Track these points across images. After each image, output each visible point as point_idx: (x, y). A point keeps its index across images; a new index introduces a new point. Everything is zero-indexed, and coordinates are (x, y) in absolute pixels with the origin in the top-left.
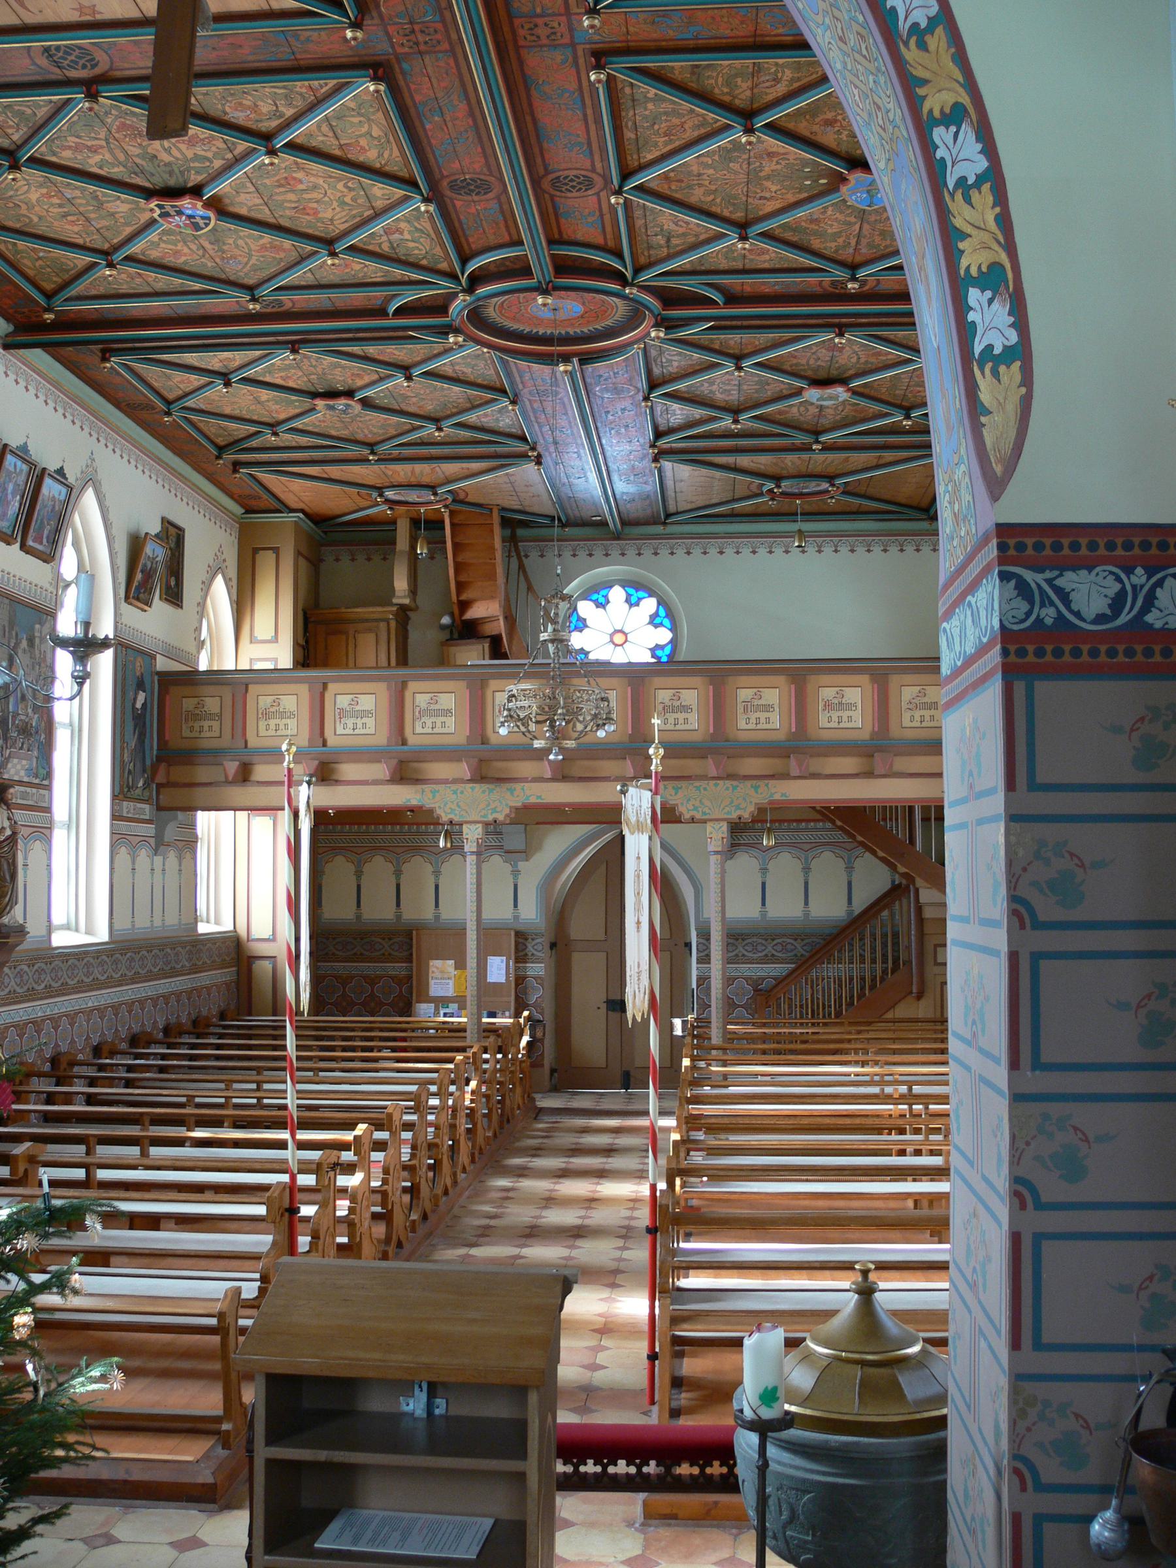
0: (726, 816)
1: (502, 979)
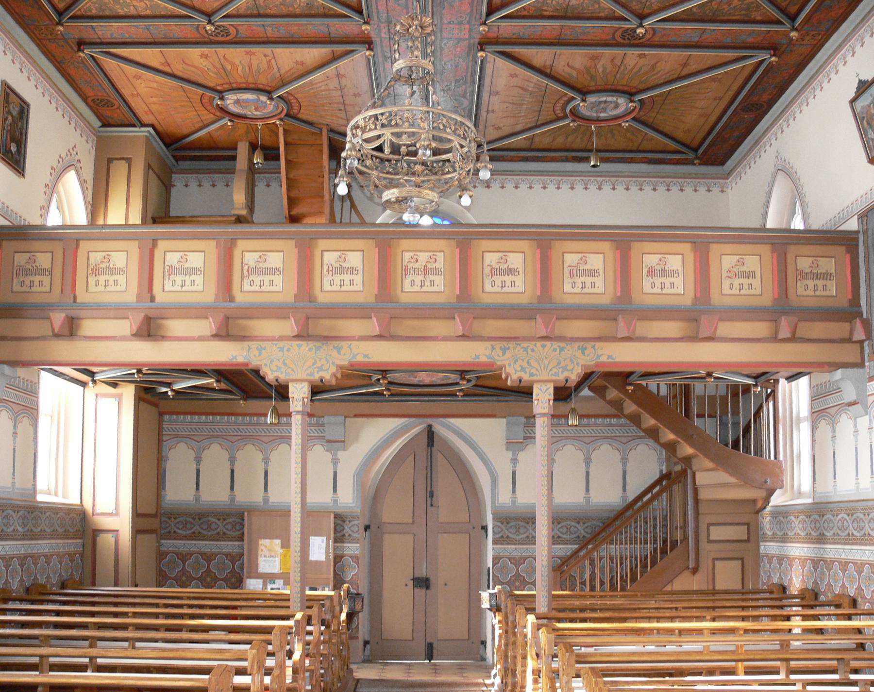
0: (554, 378)
1: (323, 558)
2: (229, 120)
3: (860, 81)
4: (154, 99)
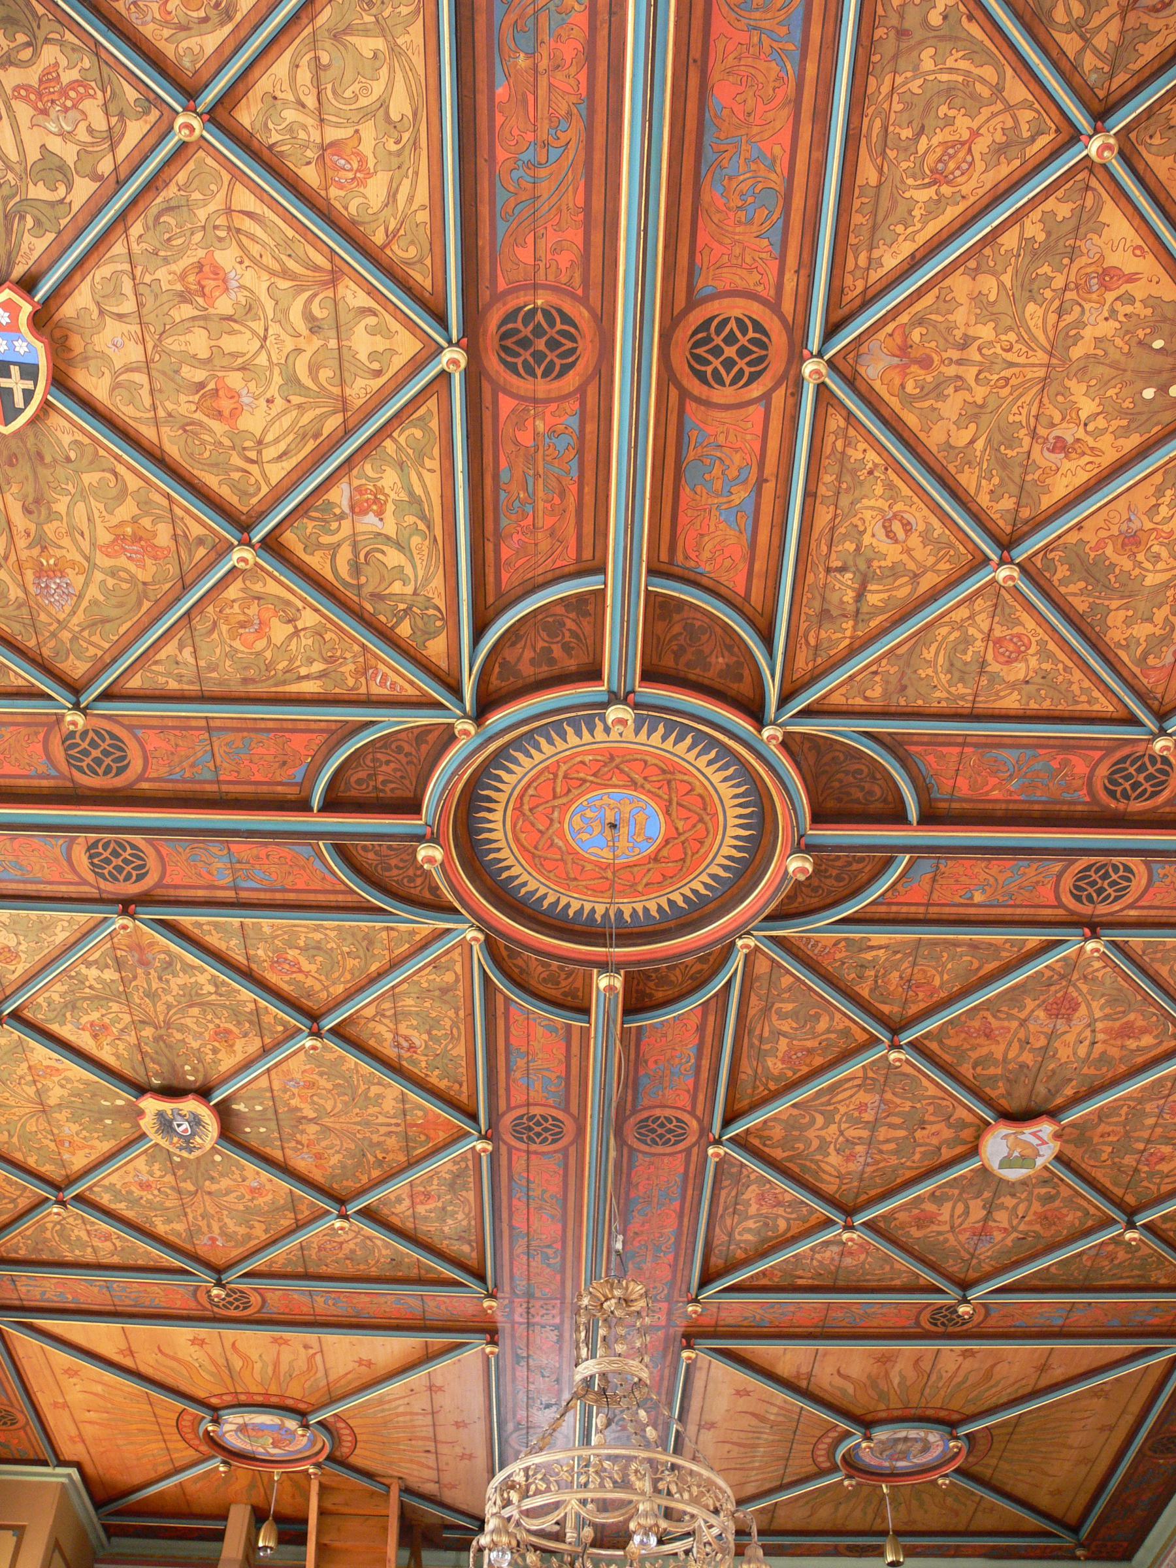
2: (224, 1462)
4: (93, 1416)
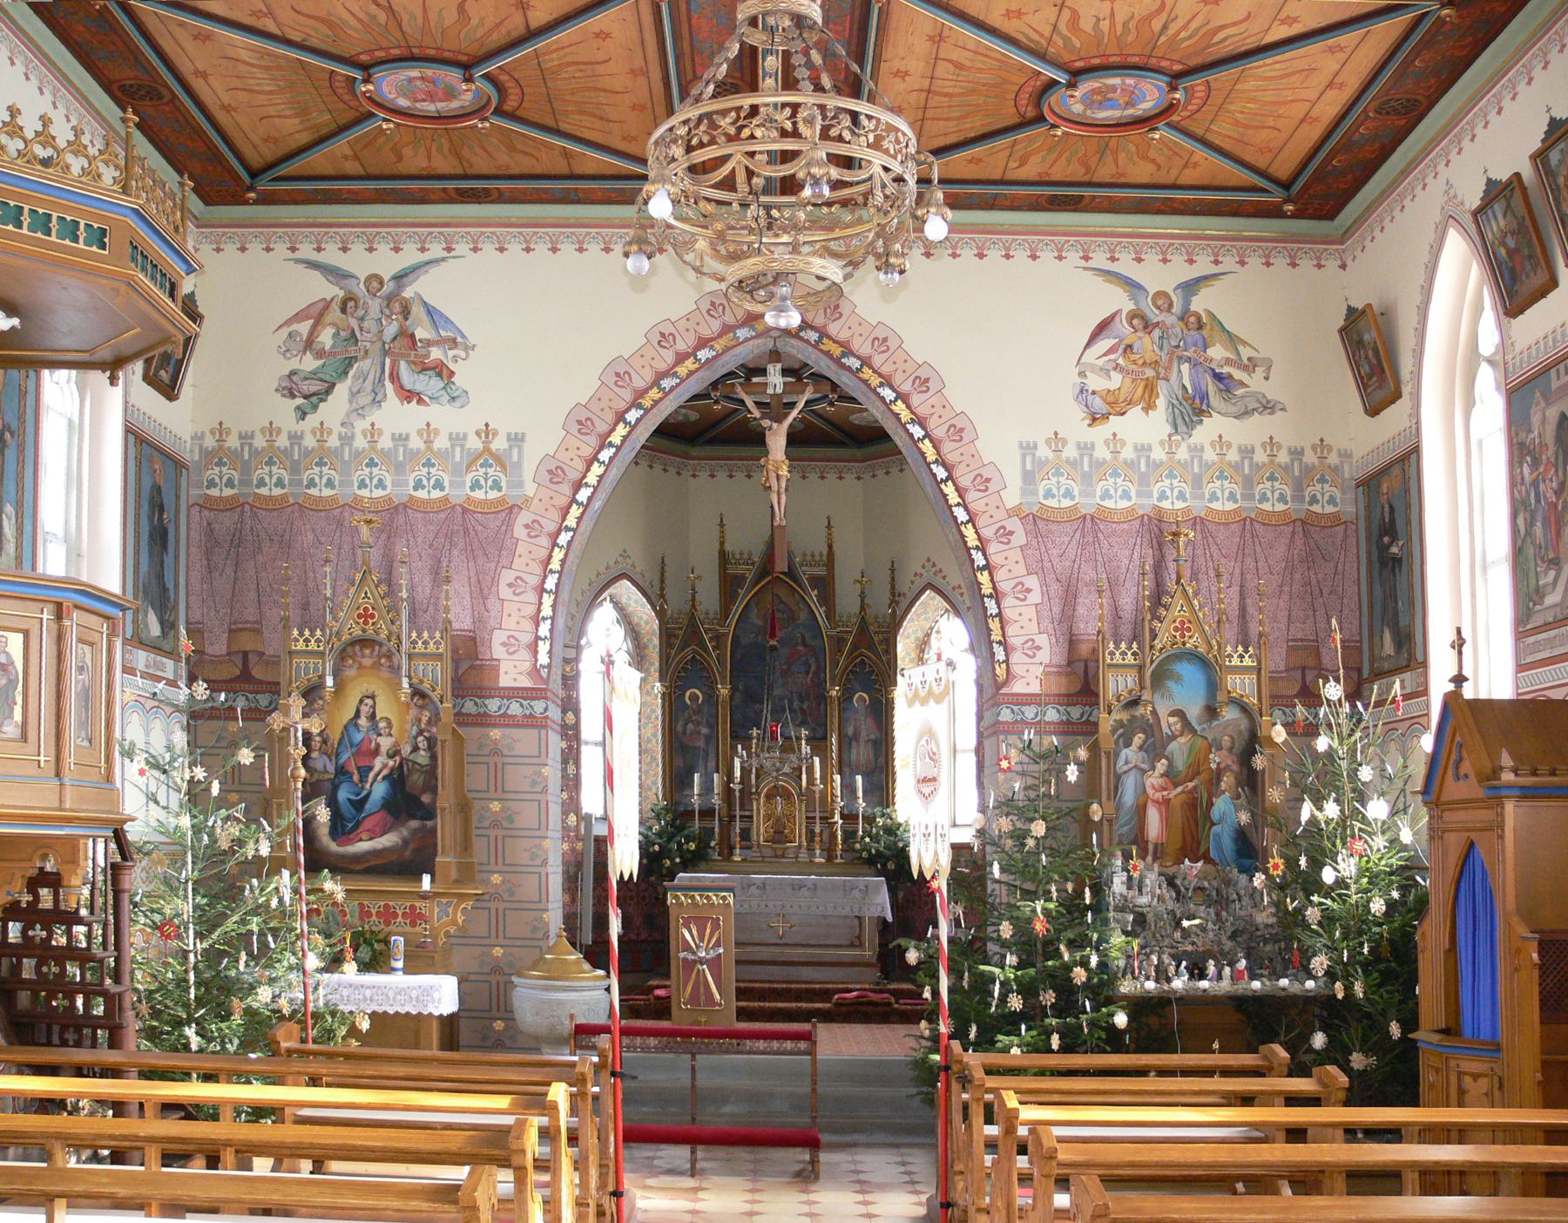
3: (1489, 181)
